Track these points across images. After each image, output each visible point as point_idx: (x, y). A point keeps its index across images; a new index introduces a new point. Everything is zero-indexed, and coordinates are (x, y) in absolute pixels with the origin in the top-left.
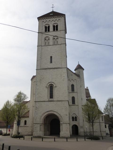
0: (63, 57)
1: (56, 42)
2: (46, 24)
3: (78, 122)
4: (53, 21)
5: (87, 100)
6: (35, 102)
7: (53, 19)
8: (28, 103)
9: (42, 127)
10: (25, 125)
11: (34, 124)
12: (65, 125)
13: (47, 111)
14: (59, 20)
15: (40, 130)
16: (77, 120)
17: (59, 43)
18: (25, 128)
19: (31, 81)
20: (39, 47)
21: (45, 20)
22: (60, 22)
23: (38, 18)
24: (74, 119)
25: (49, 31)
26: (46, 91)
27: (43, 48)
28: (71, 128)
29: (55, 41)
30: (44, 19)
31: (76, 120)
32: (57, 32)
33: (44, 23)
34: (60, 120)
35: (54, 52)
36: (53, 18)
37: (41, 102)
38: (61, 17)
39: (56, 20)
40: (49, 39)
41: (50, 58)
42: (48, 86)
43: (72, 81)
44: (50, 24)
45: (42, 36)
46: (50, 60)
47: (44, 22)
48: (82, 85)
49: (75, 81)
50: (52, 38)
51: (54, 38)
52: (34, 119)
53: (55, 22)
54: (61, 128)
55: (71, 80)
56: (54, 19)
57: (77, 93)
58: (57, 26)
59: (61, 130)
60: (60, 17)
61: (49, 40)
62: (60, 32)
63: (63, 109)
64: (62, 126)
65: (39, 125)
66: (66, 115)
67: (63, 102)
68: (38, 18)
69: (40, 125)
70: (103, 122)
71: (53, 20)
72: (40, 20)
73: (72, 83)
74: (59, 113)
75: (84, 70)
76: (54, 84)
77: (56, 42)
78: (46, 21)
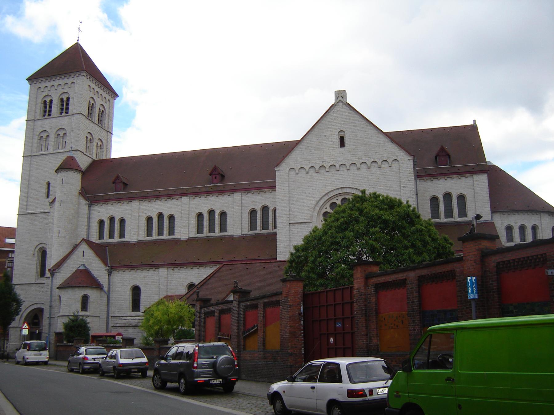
21: (43, 85)
58: (68, 99)
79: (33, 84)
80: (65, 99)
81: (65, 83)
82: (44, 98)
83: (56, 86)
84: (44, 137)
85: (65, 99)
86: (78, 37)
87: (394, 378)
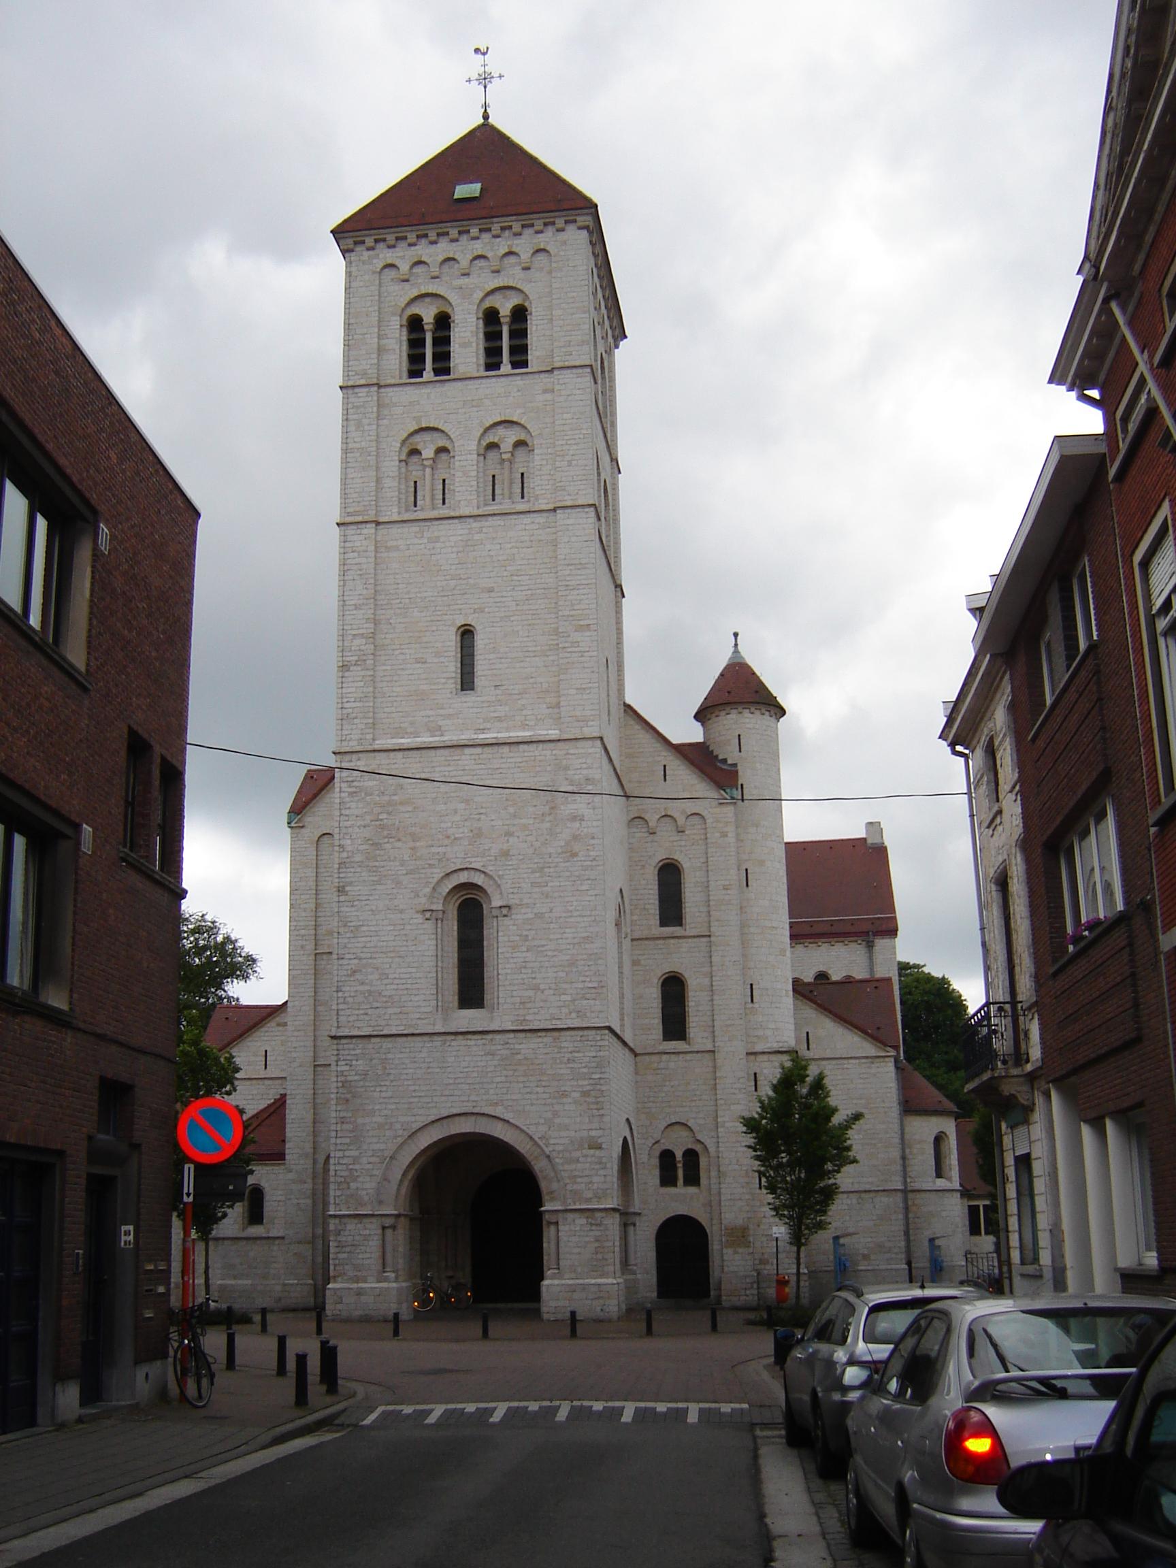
1: (511, 482)
2: (415, 293)
3: (709, 1189)
5: (800, 989)
7: (478, 247)
8: (271, 1025)
9: (400, 1240)
12: (581, 1221)
16: (703, 1181)
20: (351, 530)
21: (402, 256)
24: (680, 1173)
25: (443, 367)
26: (428, 945)
27: (397, 548)
28: (652, 1244)
31: (693, 1179)
32: (518, 382)
33: (395, 288)
34: (543, 1185)
35: (491, 590)
36: (486, 237)
40: (442, 450)
41: (452, 641)
42: (440, 907)
43: (666, 832)
44: (453, 297)
46: (452, 667)
50: (473, 446)
51: (491, 438)
52: (326, 1170)
54: (548, 1246)
55: (652, 819)
56: (492, 246)
57: (269, 1317)
58: (520, 314)
60: (550, 231)
61: (444, 456)
63: (564, 1094)
64: (558, 1231)
65: (373, 1227)
66: (590, 1148)
69: (384, 1228)
70: (941, 1183)
72: (359, 248)
73: (664, 847)
77: (511, 482)
79: (362, 254)
80: (505, 310)
81: (389, 261)
82: (417, 303)
83: (525, 256)
84: (507, 446)
85: (505, 310)
86: (501, 76)
87: (713, 1405)
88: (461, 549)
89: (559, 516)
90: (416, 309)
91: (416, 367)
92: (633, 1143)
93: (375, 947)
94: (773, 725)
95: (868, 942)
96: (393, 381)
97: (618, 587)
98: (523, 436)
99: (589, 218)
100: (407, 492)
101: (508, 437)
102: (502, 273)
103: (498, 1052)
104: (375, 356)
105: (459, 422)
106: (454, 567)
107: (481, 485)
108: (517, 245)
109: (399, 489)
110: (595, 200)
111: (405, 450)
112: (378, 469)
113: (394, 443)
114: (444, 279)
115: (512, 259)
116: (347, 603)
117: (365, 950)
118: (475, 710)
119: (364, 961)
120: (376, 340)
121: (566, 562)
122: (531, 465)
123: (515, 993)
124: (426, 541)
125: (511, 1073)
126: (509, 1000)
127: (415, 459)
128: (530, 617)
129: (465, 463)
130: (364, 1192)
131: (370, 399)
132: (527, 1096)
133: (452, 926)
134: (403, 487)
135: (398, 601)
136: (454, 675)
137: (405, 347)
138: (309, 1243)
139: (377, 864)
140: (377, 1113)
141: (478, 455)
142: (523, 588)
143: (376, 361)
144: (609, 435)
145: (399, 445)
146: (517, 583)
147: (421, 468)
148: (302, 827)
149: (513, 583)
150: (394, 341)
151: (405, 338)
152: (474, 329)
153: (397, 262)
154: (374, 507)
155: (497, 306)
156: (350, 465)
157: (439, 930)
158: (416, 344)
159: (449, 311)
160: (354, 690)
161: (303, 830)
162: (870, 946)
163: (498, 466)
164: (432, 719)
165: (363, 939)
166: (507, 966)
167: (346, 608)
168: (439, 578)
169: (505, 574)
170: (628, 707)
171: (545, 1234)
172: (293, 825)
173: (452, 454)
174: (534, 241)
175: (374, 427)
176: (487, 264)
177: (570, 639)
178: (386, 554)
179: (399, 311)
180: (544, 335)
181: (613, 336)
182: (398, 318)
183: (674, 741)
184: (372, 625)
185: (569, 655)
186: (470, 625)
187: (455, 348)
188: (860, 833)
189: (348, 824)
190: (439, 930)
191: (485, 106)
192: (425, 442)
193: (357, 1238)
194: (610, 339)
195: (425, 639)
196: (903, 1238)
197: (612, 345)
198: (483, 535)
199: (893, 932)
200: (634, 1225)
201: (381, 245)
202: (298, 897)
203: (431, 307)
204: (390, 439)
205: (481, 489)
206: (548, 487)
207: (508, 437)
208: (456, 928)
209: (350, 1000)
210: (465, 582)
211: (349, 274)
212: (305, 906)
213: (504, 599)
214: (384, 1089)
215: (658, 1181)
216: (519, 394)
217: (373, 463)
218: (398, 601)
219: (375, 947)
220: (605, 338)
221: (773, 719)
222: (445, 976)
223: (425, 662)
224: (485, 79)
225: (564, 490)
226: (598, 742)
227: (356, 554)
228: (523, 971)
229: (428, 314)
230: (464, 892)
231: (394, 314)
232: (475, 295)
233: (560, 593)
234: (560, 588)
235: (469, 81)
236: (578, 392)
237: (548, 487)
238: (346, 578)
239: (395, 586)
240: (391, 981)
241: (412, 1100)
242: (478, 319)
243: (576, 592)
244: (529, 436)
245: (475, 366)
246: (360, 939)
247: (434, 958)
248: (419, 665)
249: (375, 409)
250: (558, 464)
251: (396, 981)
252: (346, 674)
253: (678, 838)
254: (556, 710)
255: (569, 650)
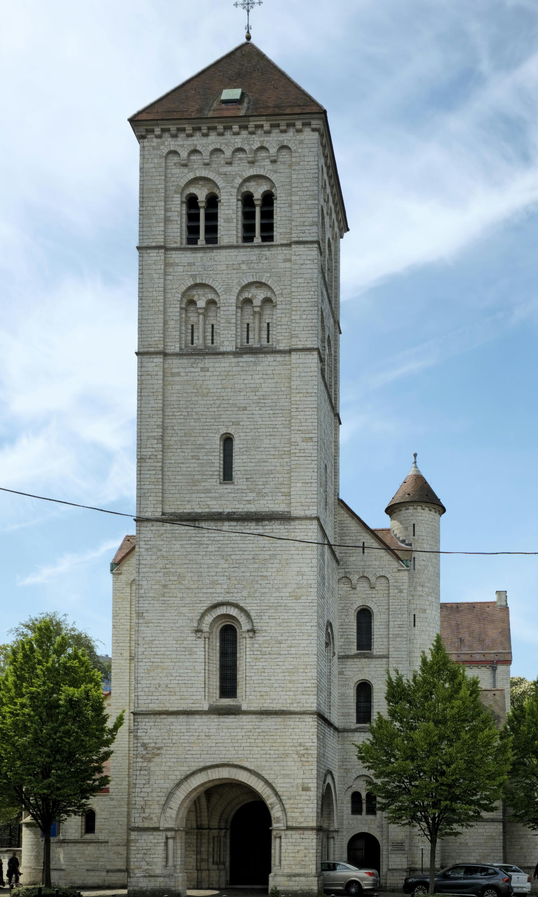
0: (303, 445)
1: (260, 330)
2: (191, 176)
4: (241, 155)
6: (135, 714)
7: (238, 141)
10: (89, 836)
11: (135, 833)
13: (202, 765)
14: (284, 156)
15: (109, 867)
17: (278, 341)
18: (90, 849)
19: (111, 576)
20: (146, 359)
22: (290, 166)
23: (134, 121)
24: (364, 806)
26: (200, 654)
27: (178, 374)
29: (255, 324)
30: (182, 135)
32: (267, 252)
33: (176, 171)
36: (244, 133)
37: (171, 719)
38: (299, 131)
39: (262, 148)
41: (217, 444)
43: (362, 587)
44: (220, 183)
45: (165, 274)
47: (175, 159)
48: (424, 611)
49: (381, 585)
50: (233, 300)
53: (252, 163)
59: (277, 863)
60: (291, 132)
61: (213, 308)
62: (285, 251)
64: (281, 842)
67: (292, 721)
68: (134, 121)
69: (167, 838)
71: (241, 150)
74: (266, 777)
75: (442, 510)
76: (242, 619)
77: (260, 330)
78: (195, 151)
80: (258, 195)
81: (172, 148)
84: (257, 302)
85: (258, 195)
86: (260, 3)
88: (224, 377)
89: (293, 356)
90: (193, 190)
91: (192, 237)
92: (335, 788)
93: (163, 655)
94: (436, 518)
95: (493, 667)
96: (175, 245)
97: (337, 415)
98: (269, 294)
99: (320, 122)
100: (187, 332)
101: (259, 295)
102: (256, 164)
103: (245, 727)
104: (162, 224)
105: (224, 281)
106: (219, 391)
107: (239, 330)
108: (267, 141)
109: (180, 330)
110: (325, 107)
111: (185, 300)
112: (165, 312)
113: (177, 295)
114: (213, 166)
115: (264, 154)
116: (143, 413)
117: (156, 656)
118: (233, 495)
119: (156, 664)
120: (163, 212)
121: (298, 391)
122: (275, 317)
123: (256, 689)
124: (199, 370)
125: (253, 741)
126: (253, 693)
127: (192, 308)
128: (271, 430)
129: (227, 313)
130: (155, 815)
131: (159, 258)
132: (264, 756)
133: (217, 643)
134: (183, 328)
135: (180, 413)
136: (218, 469)
137: (184, 219)
138: (124, 845)
139: (165, 598)
140: (164, 764)
141: (237, 307)
142: (267, 409)
143: (163, 229)
144: (333, 303)
145: (180, 296)
146: (263, 405)
147: (196, 315)
148: (121, 574)
149: (260, 405)
150: (176, 214)
151: (184, 212)
152: (235, 208)
153: (179, 150)
154: (162, 342)
155: (252, 190)
156: (144, 309)
157: (207, 645)
158: (193, 218)
159: (217, 192)
160: (148, 476)
161: (120, 576)
162: (494, 670)
163: (252, 317)
164: (202, 500)
165: (156, 649)
166: (252, 671)
167: (143, 416)
168: (208, 398)
169: (255, 398)
170: (341, 501)
171: (273, 844)
172: (114, 571)
173: (218, 305)
174: (281, 139)
175: (162, 281)
176: (245, 156)
177: (298, 447)
178: (171, 378)
179: (180, 190)
180: (285, 216)
181: (339, 227)
182: (179, 196)
183: (372, 527)
184: (161, 430)
185: (297, 458)
186: (230, 434)
187: (221, 222)
188: (493, 598)
189: (144, 570)
190: (207, 645)
191: (248, 28)
192: (199, 295)
193: (149, 844)
194: (336, 229)
195: (198, 443)
196: (502, 851)
197: (338, 235)
198: (239, 369)
199: (508, 662)
200: (334, 838)
201: (166, 135)
202: (117, 621)
203: (203, 188)
204: (173, 291)
205: (239, 334)
206: (286, 334)
207: (259, 295)
208: (218, 644)
209: (147, 689)
210: (227, 402)
211: (142, 156)
212: (123, 627)
213: (253, 416)
214: (169, 748)
215: (350, 812)
216: (267, 261)
217: (161, 308)
218: (180, 413)
219: (163, 655)
220: (332, 226)
221: (437, 514)
222: (211, 676)
223: (199, 459)
224: (248, 4)
225: (297, 337)
226: (315, 522)
227: (150, 377)
228: (263, 674)
229: (202, 194)
230: (224, 620)
231: (176, 192)
232: (236, 181)
233: (293, 414)
234: (292, 410)
235: (236, 5)
236: (309, 262)
237: (286, 334)
238: (143, 394)
239: (178, 402)
240: (174, 678)
241: (186, 756)
242: (238, 200)
243: (302, 413)
244: (273, 295)
245: (235, 237)
246: (153, 649)
247: (203, 664)
248: (194, 461)
249: (163, 267)
250: (293, 317)
251: (177, 678)
252: (143, 464)
253: (371, 592)
254: (288, 498)
255: (297, 455)
